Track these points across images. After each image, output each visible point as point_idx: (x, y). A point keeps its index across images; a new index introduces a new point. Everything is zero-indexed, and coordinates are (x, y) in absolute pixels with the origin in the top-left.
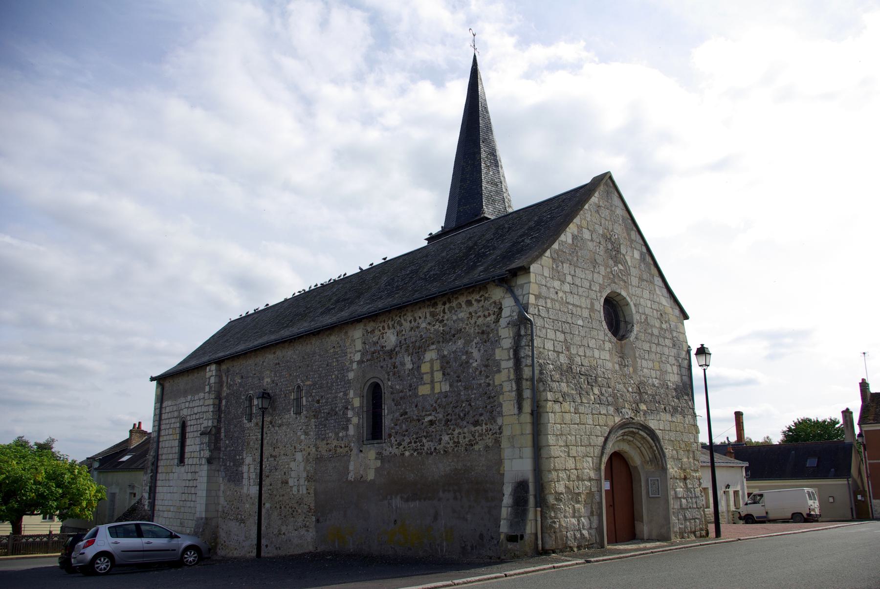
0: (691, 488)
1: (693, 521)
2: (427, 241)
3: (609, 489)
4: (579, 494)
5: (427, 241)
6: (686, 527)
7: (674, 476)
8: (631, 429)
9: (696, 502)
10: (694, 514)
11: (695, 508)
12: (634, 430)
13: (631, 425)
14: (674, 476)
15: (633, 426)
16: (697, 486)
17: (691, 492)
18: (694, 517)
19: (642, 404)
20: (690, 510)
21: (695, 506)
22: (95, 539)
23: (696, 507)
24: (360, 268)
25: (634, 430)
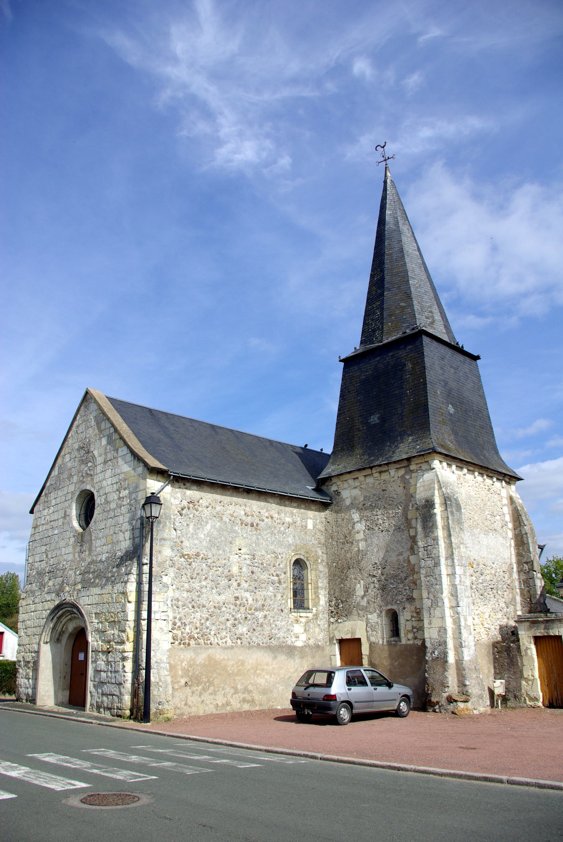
0: (112, 661)
1: (110, 697)
2: (343, 363)
3: (83, 659)
4: (29, 662)
5: (343, 363)
6: (102, 702)
7: (96, 649)
8: (67, 609)
9: (115, 677)
10: (112, 690)
11: (113, 683)
12: (69, 609)
13: (65, 606)
14: (96, 649)
15: (67, 606)
16: (118, 659)
17: (111, 666)
18: (111, 693)
19: (404, 472)
20: (108, 684)
21: (113, 681)
22: (367, 685)
23: (114, 682)
24: (322, 450)
25: (69, 609)
